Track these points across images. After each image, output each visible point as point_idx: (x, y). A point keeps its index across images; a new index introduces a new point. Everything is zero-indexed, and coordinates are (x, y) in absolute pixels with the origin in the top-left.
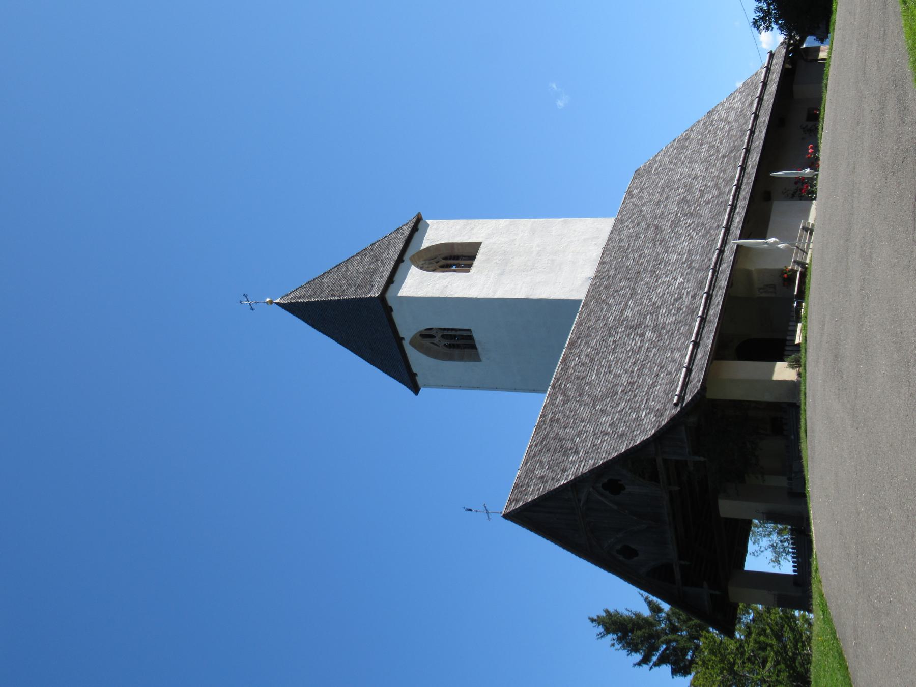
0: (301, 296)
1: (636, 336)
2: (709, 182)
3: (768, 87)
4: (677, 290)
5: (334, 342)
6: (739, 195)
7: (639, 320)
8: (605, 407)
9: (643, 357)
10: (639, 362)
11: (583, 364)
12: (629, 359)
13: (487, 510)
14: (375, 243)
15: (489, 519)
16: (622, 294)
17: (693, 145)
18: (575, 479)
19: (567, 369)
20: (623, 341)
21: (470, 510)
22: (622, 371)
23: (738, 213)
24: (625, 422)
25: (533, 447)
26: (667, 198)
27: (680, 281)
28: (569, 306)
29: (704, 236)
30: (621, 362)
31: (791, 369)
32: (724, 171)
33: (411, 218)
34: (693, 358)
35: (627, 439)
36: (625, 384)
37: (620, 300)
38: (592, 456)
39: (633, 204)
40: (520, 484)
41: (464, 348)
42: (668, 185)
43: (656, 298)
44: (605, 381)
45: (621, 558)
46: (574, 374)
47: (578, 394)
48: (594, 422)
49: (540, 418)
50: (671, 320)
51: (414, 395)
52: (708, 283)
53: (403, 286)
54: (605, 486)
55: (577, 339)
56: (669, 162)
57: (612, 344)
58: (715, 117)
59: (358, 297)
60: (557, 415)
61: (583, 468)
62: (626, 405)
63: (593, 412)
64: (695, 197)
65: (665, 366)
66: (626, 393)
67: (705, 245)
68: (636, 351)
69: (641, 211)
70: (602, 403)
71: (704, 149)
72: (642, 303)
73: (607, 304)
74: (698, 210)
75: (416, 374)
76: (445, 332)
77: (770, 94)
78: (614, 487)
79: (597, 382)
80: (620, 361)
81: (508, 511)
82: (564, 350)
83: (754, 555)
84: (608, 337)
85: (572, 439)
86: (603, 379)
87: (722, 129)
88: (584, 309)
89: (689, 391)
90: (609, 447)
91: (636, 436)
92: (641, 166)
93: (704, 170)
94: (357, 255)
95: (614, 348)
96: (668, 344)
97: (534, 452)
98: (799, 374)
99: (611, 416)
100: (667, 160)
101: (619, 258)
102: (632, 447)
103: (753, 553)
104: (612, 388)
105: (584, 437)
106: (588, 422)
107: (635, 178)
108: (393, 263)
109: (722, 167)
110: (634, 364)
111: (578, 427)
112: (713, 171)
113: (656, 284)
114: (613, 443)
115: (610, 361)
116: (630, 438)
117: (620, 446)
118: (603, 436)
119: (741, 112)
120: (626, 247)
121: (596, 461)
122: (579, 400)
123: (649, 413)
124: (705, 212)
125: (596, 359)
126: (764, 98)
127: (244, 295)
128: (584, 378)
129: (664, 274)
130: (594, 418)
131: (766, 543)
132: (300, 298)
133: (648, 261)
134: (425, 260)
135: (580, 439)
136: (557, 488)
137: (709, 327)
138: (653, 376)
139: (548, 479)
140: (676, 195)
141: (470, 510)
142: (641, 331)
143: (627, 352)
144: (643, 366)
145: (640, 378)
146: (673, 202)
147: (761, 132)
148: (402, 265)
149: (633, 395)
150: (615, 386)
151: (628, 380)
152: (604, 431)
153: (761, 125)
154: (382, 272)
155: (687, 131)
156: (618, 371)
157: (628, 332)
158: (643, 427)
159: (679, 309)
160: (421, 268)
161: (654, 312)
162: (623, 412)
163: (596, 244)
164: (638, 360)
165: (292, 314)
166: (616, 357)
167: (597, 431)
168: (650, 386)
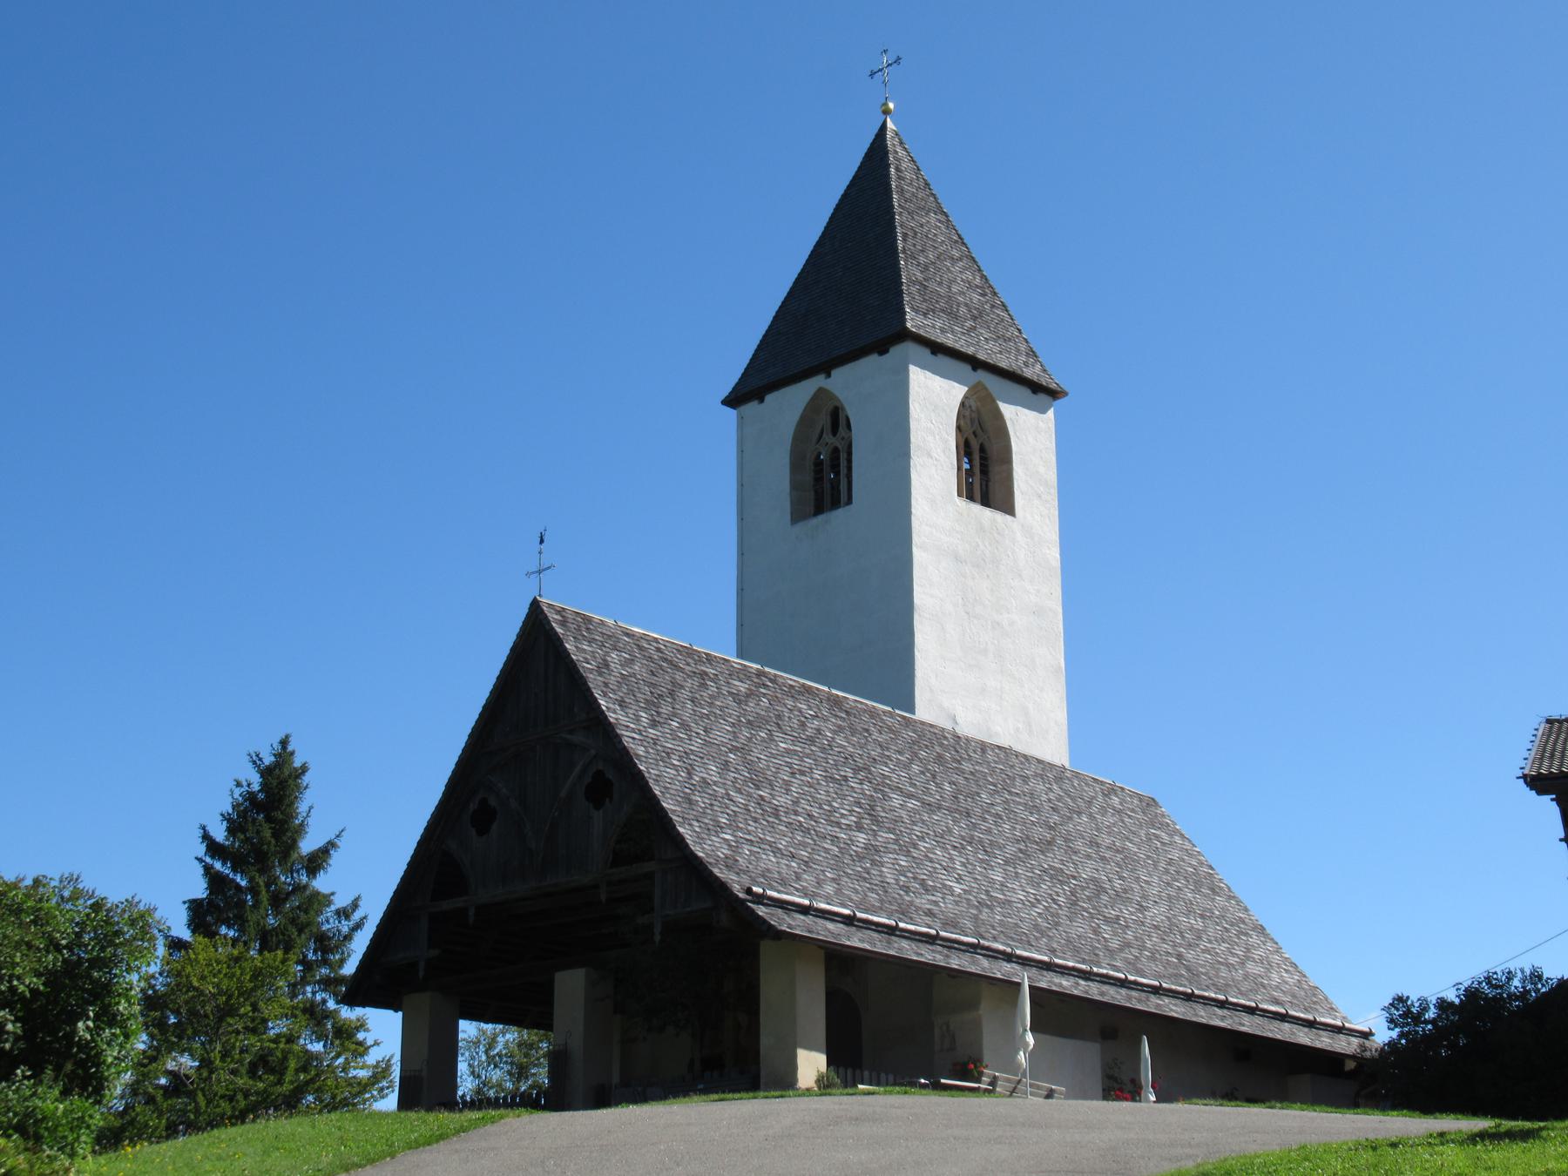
3: (1306, 1030)
7: (885, 820)
8: (733, 770)
9: (823, 830)
11: (803, 725)
13: (544, 570)
14: (1007, 311)
16: (929, 787)
18: (610, 723)
19: (792, 697)
20: (847, 793)
21: (542, 541)
22: (795, 794)
23: (1078, 984)
25: (655, 644)
26: (1103, 859)
27: (955, 889)
28: (901, 690)
29: (1036, 926)
32: (1152, 958)
33: (1056, 379)
37: (918, 783)
39: (1093, 798)
42: (1128, 861)
43: (924, 847)
44: (777, 766)
45: (473, 806)
46: (785, 710)
47: (750, 718)
49: (705, 653)
50: (889, 876)
51: (723, 398)
52: (954, 936)
54: (599, 774)
55: (846, 711)
57: (841, 776)
58: (1254, 939)
60: (712, 684)
62: (740, 805)
63: (723, 748)
64: (1107, 908)
65: (810, 870)
68: (832, 818)
73: (911, 761)
74: (1082, 915)
75: (762, 400)
77: (1293, 1033)
78: (599, 791)
79: (773, 751)
80: (812, 790)
81: (545, 608)
82: (826, 689)
84: (854, 767)
85: (675, 715)
86: (780, 762)
87: (1231, 953)
90: (668, 780)
91: (690, 825)
92: (1163, 809)
93: (1155, 923)
94: (983, 277)
99: (720, 780)
102: (671, 819)
106: (705, 740)
107: (1140, 798)
108: (970, 351)
109: (1160, 955)
110: (809, 815)
112: (1154, 939)
114: (674, 787)
115: (812, 772)
116: (686, 816)
117: (672, 799)
118: (686, 768)
120: (1013, 790)
121: (644, 759)
122: (740, 721)
123: (730, 846)
124: (1079, 928)
125: (813, 748)
127: (899, 58)
128: (780, 728)
129: (967, 859)
132: (898, 169)
133: (989, 831)
136: (592, 693)
141: (542, 541)
144: (807, 831)
145: (786, 827)
146: (1097, 870)
147: (1223, 1018)
148: (966, 368)
149: (758, 816)
153: (1235, 1018)
155: (1229, 889)
156: (796, 788)
157: (863, 801)
159: (907, 889)
160: (963, 404)
161: (900, 845)
162: (727, 801)
163: (1018, 729)
164: (815, 822)
166: (819, 784)
167: (692, 757)
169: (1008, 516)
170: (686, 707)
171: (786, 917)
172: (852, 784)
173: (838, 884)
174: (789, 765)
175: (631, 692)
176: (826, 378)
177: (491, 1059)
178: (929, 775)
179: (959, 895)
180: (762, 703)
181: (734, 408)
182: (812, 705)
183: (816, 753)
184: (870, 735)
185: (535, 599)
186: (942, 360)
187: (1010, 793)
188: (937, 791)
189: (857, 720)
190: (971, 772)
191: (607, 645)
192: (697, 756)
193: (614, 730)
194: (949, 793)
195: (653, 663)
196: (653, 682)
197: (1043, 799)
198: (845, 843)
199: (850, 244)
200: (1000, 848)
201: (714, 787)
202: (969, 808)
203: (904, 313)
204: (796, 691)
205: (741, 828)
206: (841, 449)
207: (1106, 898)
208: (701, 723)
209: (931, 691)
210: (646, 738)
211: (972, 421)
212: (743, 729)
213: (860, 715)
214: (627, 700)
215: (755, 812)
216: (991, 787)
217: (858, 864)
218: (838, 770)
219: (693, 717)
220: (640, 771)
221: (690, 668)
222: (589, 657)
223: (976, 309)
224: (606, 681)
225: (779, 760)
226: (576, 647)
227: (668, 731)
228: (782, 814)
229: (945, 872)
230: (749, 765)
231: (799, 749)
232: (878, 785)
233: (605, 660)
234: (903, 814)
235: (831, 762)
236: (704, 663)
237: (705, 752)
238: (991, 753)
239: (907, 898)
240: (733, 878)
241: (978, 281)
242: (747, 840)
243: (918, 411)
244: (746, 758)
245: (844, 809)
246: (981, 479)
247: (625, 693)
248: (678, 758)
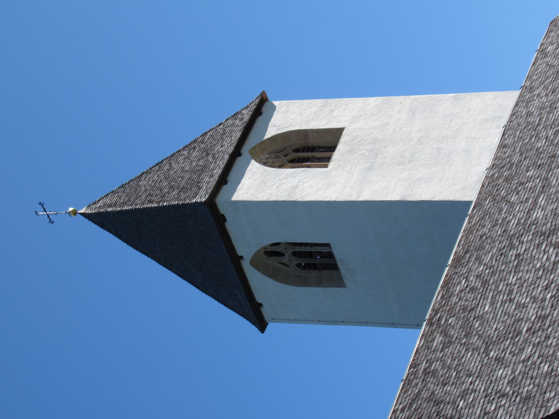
0: (111, 204)
5: (155, 263)
7: (554, 224)
8: (503, 353)
10: (553, 285)
11: (472, 289)
14: (207, 133)
16: (529, 188)
19: (450, 297)
20: (529, 255)
22: (528, 299)
24: (532, 378)
25: (398, 413)
30: (527, 286)
33: (252, 98)
35: (534, 405)
39: (547, 65)
41: (323, 269)
46: (460, 303)
47: (463, 334)
48: (486, 376)
49: (410, 369)
51: (259, 332)
53: (238, 188)
55: (465, 253)
57: (515, 260)
59: (181, 203)
60: (434, 366)
62: (534, 350)
63: (485, 362)
66: (534, 332)
68: (550, 268)
70: (498, 347)
73: (508, 202)
75: (260, 305)
76: (298, 247)
79: (491, 316)
80: (525, 285)
82: (447, 269)
84: (509, 248)
85: (454, 403)
88: (475, 211)
91: (548, 400)
94: (184, 149)
95: (517, 265)
99: (511, 367)
101: (527, 138)
104: (513, 324)
105: (471, 400)
106: (477, 377)
107: (550, 31)
108: (227, 157)
110: (546, 289)
111: (463, 383)
114: (514, 412)
115: (511, 284)
116: (540, 403)
118: (499, 398)
120: (537, 123)
122: (465, 343)
125: (491, 282)
130: (486, 370)
132: (110, 206)
134: (269, 153)
135: (466, 403)
143: (535, 271)
145: (555, 310)
148: (239, 160)
149: (544, 335)
150: (518, 322)
151: (537, 312)
152: (500, 391)
154: (213, 169)
156: (522, 299)
157: (537, 241)
160: (265, 164)
162: (529, 363)
164: (552, 283)
165: (102, 227)
166: (520, 279)
167: (490, 391)
169: (343, 133)
172: (523, 250)
174: (503, 303)
176: (244, 260)
178: (520, 188)
180: (453, 323)
181: (267, 324)
182: (458, 281)
183: (495, 280)
184: (485, 234)
186: (231, 177)
187: (538, 125)
188: (533, 181)
189: (473, 245)
190: (520, 155)
192: (489, 387)
194: (536, 172)
197: (545, 101)
201: (517, 373)
202: (548, 155)
203: (196, 202)
204: (446, 293)
205: (554, 351)
206: (294, 250)
211: (277, 157)
212: (471, 341)
213: (469, 242)
215: (540, 337)
216: (533, 139)
218: (510, 262)
219: (457, 386)
221: (420, 384)
223: (202, 154)
225: (498, 311)
228: (543, 313)
230: (501, 338)
231: (491, 294)
232: (524, 229)
234: (549, 208)
235: (454, 276)
236: (417, 371)
237: (486, 378)
238: (507, 141)
241: (185, 153)
243: (264, 194)
244: (495, 342)
245: (542, 258)
246: (317, 152)
248: (489, 405)
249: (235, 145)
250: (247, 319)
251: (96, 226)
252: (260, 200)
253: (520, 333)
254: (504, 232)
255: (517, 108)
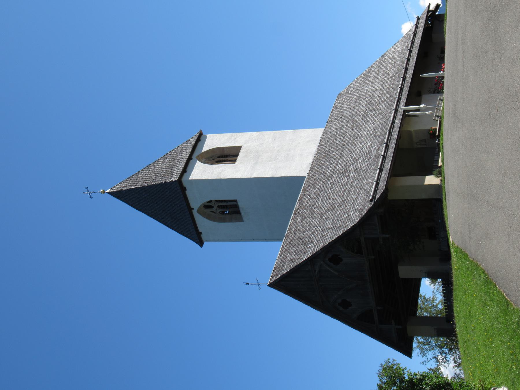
1: (345, 177)
2: (384, 91)
3: (417, 35)
4: (368, 149)
6: (402, 93)
7: (346, 169)
8: (328, 216)
9: (349, 187)
10: (347, 190)
12: (341, 190)
13: (258, 283)
14: (172, 150)
15: (260, 289)
17: (374, 74)
18: (312, 255)
19: (303, 203)
20: (336, 181)
21: (248, 284)
24: (341, 220)
26: (359, 105)
27: (370, 144)
28: (299, 180)
31: (437, 178)
34: (379, 178)
36: (339, 202)
38: (322, 241)
39: (338, 112)
40: (278, 267)
42: (359, 98)
43: (355, 156)
44: (327, 203)
45: (341, 308)
46: (307, 205)
47: (311, 214)
49: (288, 231)
50: (365, 164)
51: (200, 247)
52: (386, 138)
54: (330, 260)
55: (308, 187)
56: (359, 86)
57: (330, 185)
58: (386, 57)
60: (298, 228)
61: (317, 249)
62: (341, 212)
64: (376, 100)
65: (363, 187)
67: (384, 123)
69: (343, 114)
71: (380, 76)
72: (347, 160)
74: (378, 107)
75: (201, 233)
77: (418, 38)
78: (336, 260)
80: (335, 192)
81: (272, 282)
82: (300, 194)
83: (424, 364)
86: (326, 203)
87: (391, 63)
89: (378, 193)
90: (332, 234)
91: (348, 225)
92: (342, 92)
93: (381, 86)
96: (364, 176)
97: (285, 249)
98: (441, 180)
99: (332, 219)
100: (357, 85)
102: (346, 231)
103: (423, 362)
106: (318, 226)
107: (338, 98)
108: (185, 160)
109: (392, 82)
110: (344, 191)
112: (386, 85)
113: (355, 149)
114: (334, 232)
117: (339, 232)
119: (401, 52)
121: (325, 243)
123: (355, 212)
126: (415, 41)
128: (314, 205)
129: (359, 143)
131: (431, 355)
132: (123, 187)
133: (350, 139)
134: (206, 158)
136: (301, 262)
137: (388, 160)
138: (356, 194)
139: (295, 260)
140: (365, 101)
141: (248, 284)
142: (347, 174)
144: (350, 191)
146: (363, 106)
148: (191, 162)
151: (341, 200)
155: (369, 68)
158: (352, 220)
159: (370, 158)
161: (354, 163)
163: (314, 144)
164: (346, 189)
166: (333, 190)
167: (324, 229)
168: (355, 199)
169: (242, 148)
170: (307, 234)
171: (380, 189)
173: (368, 178)
175: (301, 251)
177: (428, 344)
178: (330, 159)
179: (372, 143)
180: (305, 212)
181: (204, 243)
185: (268, 285)
191: (285, 261)
192: (323, 228)
193: (314, 254)
195: (291, 246)
196: (297, 245)
198: (354, 179)
199: (149, 203)
200: (355, 134)
205: (349, 210)
206: (218, 205)
207: (372, 101)
208: (312, 228)
209: (301, 171)
210: (317, 244)
211: (209, 160)
214: (304, 251)
215: (343, 207)
217: (361, 174)
220: (329, 243)
221: (293, 235)
222: (289, 266)
224: (297, 259)
226: (285, 270)
227: (315, 237)
228: (344, 199)
229: (364, 148)
230: (327, 211)
231: (321, 198)
233: (290, 261)
234: (343, 164)
239: (373, 157)
240: (366, 208)
241: (162, 160)
242: (353, 208)
244: (324, 213)
247: (302, 253)
249: (189, 154)
250: (194, 241)
251: (115, 198)
252: (204, 179)
253: (335, 208)
254: (325, 176)
255: (326, 130)
